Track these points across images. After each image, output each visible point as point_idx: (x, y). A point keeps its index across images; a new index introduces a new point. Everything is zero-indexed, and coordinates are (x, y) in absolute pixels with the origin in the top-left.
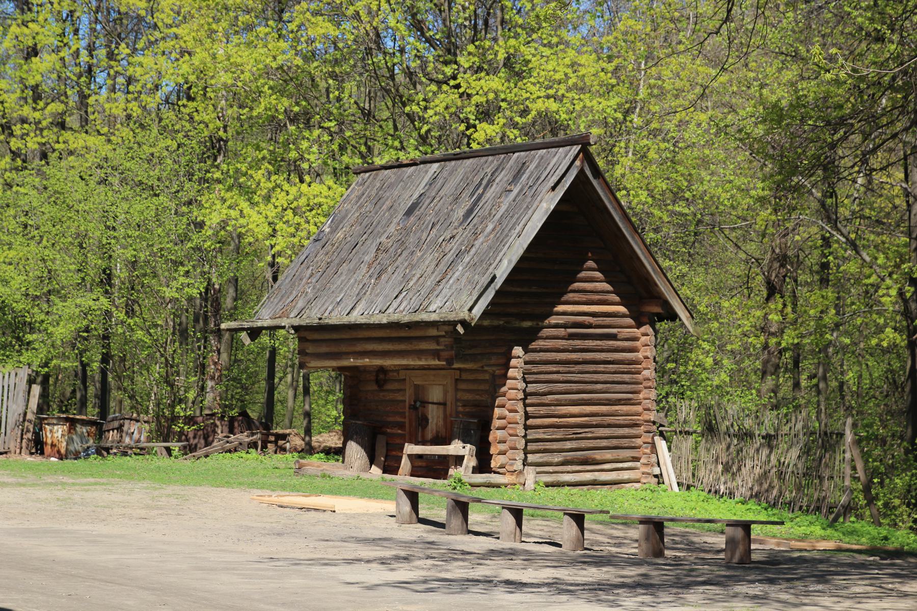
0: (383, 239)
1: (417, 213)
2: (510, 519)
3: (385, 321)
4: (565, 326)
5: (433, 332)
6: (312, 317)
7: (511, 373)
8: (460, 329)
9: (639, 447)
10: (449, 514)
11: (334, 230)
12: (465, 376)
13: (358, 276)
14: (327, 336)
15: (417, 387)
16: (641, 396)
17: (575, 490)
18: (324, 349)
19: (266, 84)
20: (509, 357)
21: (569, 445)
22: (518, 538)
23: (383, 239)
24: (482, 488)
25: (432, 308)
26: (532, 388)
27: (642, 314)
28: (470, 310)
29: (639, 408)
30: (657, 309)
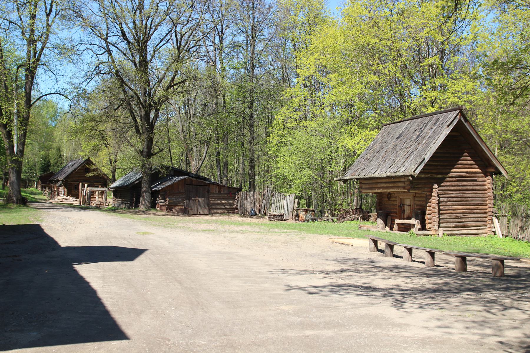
0: (388, 148)
1: (401, 138)
2: (407, 252)
3: (385, 176)
4: (455, 177)
5: (403, 180)
6: (362, 176)
7: (433, 194)
8: (410, 178)
9: (487, 221)
10: (386, 248)
11: (373, 146)
12: (417, 195)
13: (379, 161)
14: (368, 182)
15: (401, 199)
16: (487, 202)
17: (458, 237)
18: (367, 186)
19: (238, 69)
20: (432, 188)
21: (457, 220)
22: (410, 260)
23: (388, 148)
24: (422, 236)
25: (401, 171)
26: (441, 199)
27: (487, 172)
28: (414, 171)
29: (486, 207)
30: (493, 170)
